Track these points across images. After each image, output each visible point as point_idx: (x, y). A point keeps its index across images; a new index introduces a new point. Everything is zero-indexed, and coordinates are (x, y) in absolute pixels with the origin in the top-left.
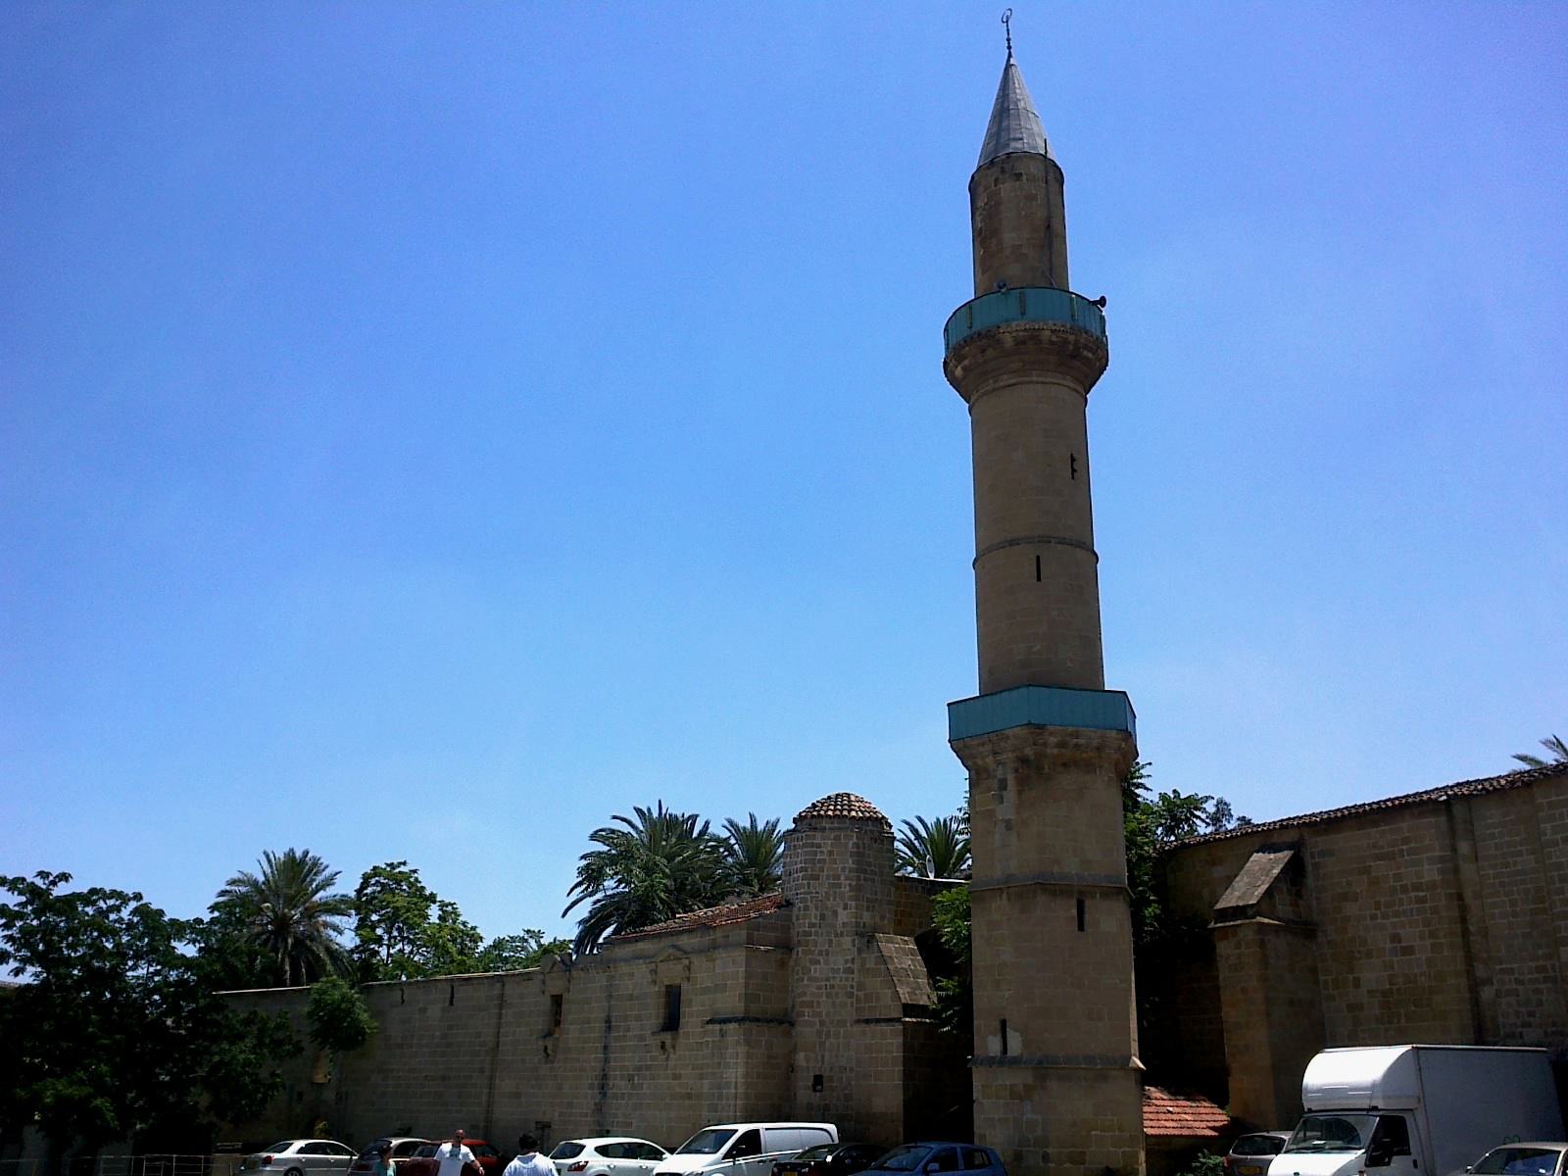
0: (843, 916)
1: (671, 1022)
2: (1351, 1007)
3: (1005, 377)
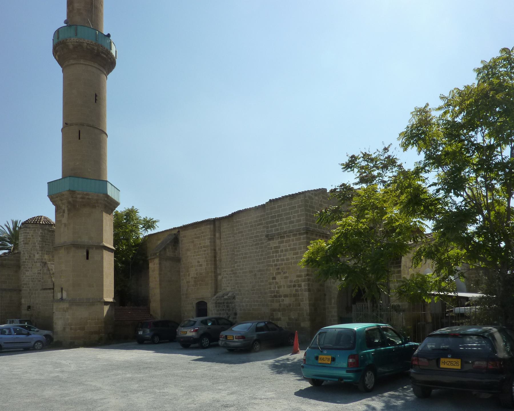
0: (37, 256)
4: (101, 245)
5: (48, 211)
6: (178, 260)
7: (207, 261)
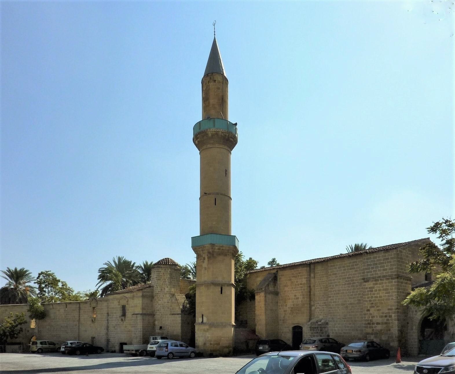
1: (124, 314)
2: (284, 311)
3: (209, 145)
4: (231, 283)
5: (186, 258)
6: (277, 294)
7: (303, 295)
